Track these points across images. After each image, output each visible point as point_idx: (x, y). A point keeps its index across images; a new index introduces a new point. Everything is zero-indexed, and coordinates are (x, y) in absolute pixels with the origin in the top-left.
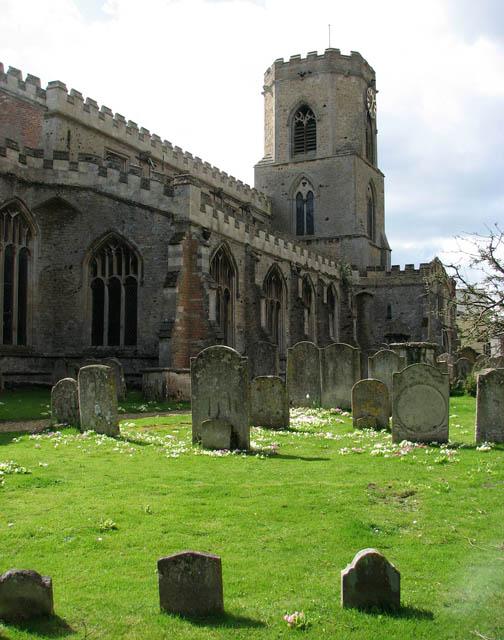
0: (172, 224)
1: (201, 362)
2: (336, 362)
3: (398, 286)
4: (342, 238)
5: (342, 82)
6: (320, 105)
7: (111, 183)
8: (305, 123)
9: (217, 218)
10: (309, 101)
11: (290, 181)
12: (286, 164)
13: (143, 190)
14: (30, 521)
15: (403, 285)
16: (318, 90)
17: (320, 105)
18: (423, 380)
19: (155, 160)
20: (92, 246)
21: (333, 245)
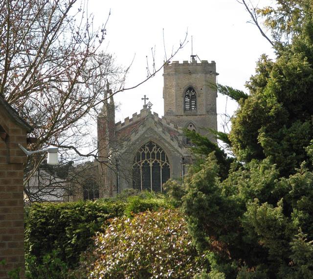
5: (209, 77)
7: (167, 137)
10: (194, 86)
12: (182, 116)
14: (65, 25)
16: (198, 80)
17: (199, 89)
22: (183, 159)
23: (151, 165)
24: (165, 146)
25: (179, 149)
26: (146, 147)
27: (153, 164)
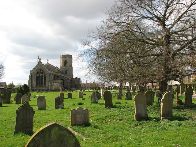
16: (67, 59)
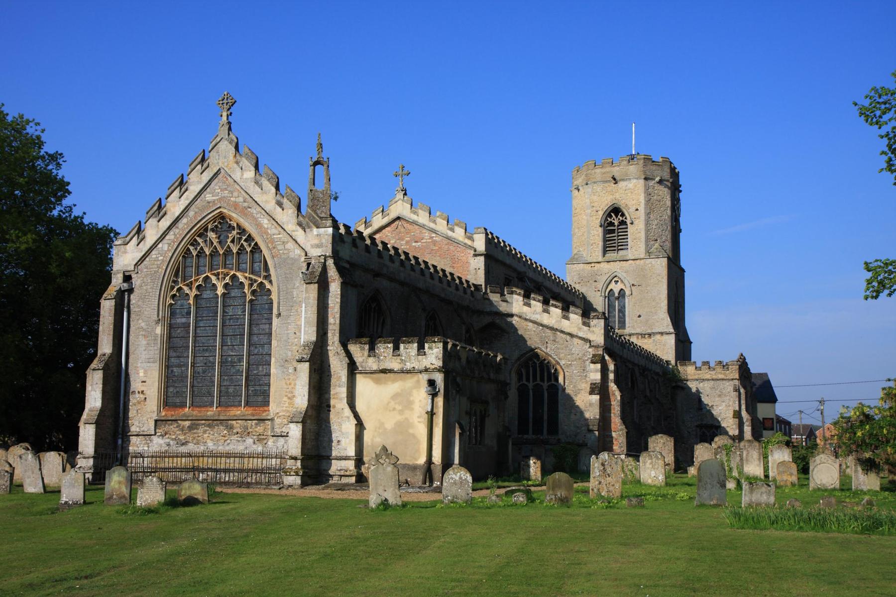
0: (590, 347)
1: (719, 450)
2: (748, 451)
3: (708, 380)
4: (654, 334)
6: (632, 209)
8: (616, 224)
9: (405, 267)
11: (603, 279)
13: (563, 320)
15: (713, 380)
17: (632, 209)
18: (825, 461)
19: (546, 288)
20: (519, 359)
21: (646, 341)
22: (309, 264)
23: (220, 291)
24: (259, 226)
25: (299, 234)
26: (212, 235)
27: (226, 286)
